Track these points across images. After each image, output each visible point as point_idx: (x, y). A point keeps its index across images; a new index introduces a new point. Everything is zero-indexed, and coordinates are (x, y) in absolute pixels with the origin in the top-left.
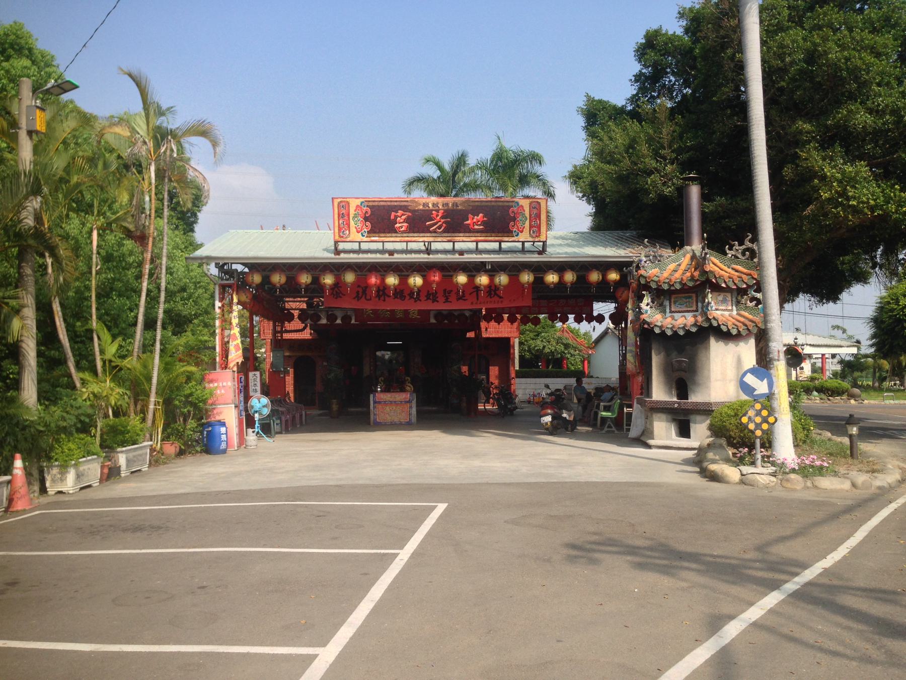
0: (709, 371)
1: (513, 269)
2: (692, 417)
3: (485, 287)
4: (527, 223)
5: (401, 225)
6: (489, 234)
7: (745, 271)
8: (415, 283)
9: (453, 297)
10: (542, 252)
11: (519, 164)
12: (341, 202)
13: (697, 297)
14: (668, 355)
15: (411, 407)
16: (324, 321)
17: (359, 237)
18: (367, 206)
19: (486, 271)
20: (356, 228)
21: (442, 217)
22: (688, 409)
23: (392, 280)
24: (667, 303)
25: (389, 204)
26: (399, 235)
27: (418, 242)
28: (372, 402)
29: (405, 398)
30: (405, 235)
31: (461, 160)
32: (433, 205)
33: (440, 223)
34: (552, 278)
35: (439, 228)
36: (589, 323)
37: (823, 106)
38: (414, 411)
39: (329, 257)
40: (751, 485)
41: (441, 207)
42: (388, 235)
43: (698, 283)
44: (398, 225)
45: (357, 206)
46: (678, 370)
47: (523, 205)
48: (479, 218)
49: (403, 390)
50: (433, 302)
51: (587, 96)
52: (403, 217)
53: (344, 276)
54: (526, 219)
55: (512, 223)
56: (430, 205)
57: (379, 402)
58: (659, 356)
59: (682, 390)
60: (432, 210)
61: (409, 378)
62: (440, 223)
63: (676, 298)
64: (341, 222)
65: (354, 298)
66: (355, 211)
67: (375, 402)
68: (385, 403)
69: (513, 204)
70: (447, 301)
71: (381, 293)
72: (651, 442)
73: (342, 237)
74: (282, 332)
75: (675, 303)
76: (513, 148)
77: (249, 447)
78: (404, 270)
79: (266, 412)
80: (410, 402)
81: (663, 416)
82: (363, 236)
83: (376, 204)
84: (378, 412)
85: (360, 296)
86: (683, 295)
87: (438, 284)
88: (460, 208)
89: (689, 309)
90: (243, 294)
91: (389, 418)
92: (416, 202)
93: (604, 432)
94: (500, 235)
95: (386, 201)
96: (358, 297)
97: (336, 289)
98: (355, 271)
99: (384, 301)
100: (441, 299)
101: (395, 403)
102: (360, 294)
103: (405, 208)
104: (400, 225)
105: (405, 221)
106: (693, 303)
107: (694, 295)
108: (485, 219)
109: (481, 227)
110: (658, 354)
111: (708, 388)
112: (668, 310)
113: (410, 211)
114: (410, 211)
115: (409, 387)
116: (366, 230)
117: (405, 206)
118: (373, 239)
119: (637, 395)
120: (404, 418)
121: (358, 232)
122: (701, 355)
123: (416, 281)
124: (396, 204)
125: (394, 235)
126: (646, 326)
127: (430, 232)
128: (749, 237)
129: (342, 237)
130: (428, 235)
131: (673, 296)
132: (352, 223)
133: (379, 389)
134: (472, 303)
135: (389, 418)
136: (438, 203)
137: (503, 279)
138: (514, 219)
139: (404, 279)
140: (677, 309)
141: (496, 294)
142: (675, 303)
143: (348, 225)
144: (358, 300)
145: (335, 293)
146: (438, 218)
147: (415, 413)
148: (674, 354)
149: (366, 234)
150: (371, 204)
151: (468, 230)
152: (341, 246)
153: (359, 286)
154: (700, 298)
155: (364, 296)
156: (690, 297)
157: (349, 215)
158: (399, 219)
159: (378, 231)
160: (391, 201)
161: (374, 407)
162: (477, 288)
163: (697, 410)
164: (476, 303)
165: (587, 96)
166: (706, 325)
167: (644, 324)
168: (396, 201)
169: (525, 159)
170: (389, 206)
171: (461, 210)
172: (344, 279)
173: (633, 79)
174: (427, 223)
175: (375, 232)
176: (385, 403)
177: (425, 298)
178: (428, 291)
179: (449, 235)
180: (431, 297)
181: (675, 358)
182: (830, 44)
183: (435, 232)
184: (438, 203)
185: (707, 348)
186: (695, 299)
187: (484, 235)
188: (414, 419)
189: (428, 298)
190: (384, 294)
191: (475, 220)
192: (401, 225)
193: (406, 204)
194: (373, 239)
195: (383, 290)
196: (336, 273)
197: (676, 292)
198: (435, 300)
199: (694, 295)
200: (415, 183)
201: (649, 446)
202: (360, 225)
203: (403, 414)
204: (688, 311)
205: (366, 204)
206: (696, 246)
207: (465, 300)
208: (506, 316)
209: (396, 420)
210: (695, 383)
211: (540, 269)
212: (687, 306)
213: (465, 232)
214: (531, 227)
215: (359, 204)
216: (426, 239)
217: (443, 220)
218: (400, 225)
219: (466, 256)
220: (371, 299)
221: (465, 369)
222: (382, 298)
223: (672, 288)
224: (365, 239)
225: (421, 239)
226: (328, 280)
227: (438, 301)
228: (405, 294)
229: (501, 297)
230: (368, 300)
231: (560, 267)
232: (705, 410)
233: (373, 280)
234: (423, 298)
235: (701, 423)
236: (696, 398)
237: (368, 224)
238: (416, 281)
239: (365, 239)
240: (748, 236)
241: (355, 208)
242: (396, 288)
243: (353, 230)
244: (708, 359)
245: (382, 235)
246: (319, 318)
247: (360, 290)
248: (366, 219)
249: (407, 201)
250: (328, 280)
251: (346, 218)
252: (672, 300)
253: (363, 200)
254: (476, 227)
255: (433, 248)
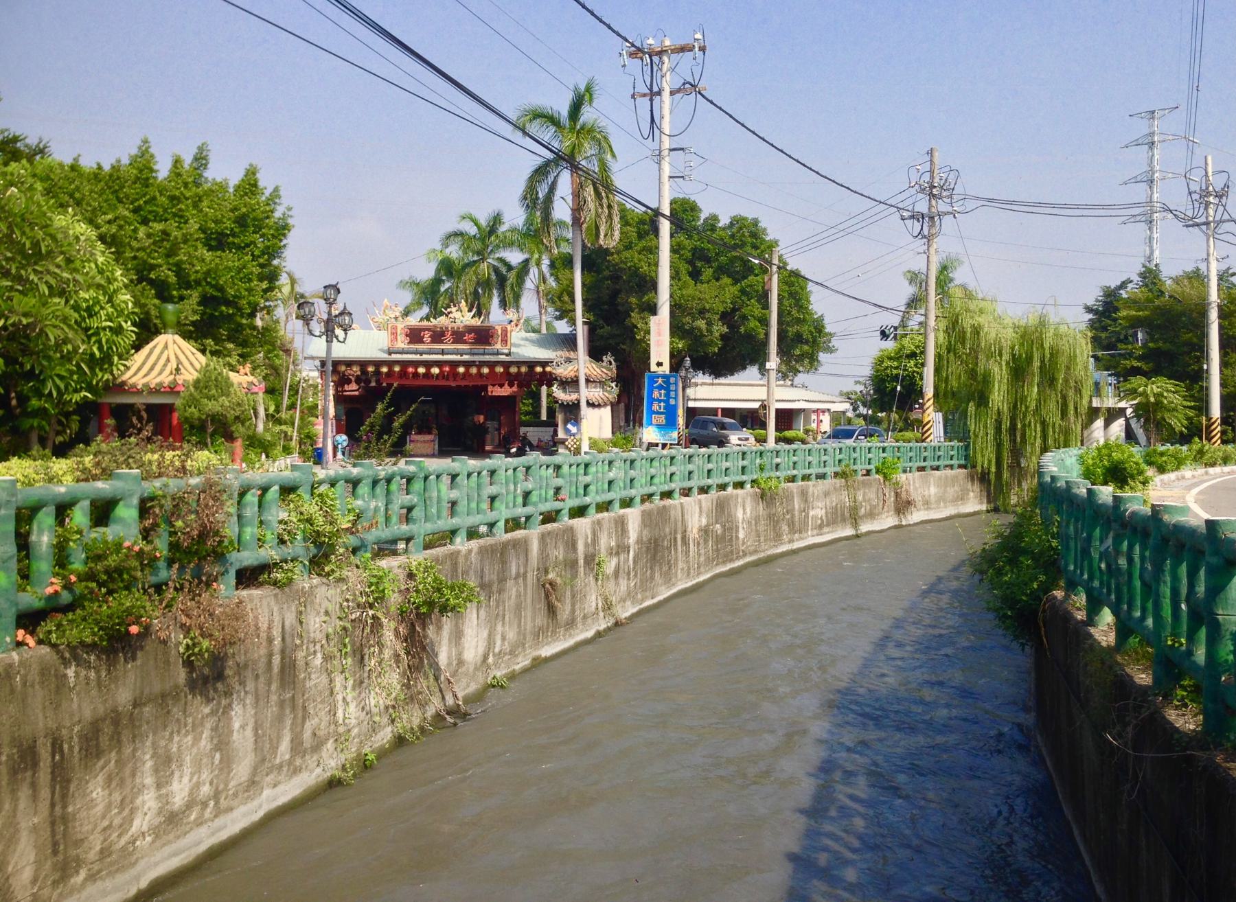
5: (427, 338)
10: (508, 355)
16: (373, 384)
19: (476, 366)
31: (497, 220)
37: (189, 563)
38: (437, 446)
39: (385, 356)
49: (430, 433)
74: (343, 391)
79: (345, 444)
100: (451, 379)
101: (424, 442)
115: (435, 431)
120: (430, 451)
123: (435, 370)
132: (399, 338)
137: (486, 370)
162: (471, 375)
182: (643, 263)
188: (436, 452)
192: (427, 338)
195: (416, 374)
200: (452, 238)
211: (507, 365)
221: (482, 418)
226: (385, 370)
231: (518, 364)
233: (411, 370)
238: (435, 370)
242: (424, 374)
246: (370, 382)
248: (407, 336)
250: (385, 370)
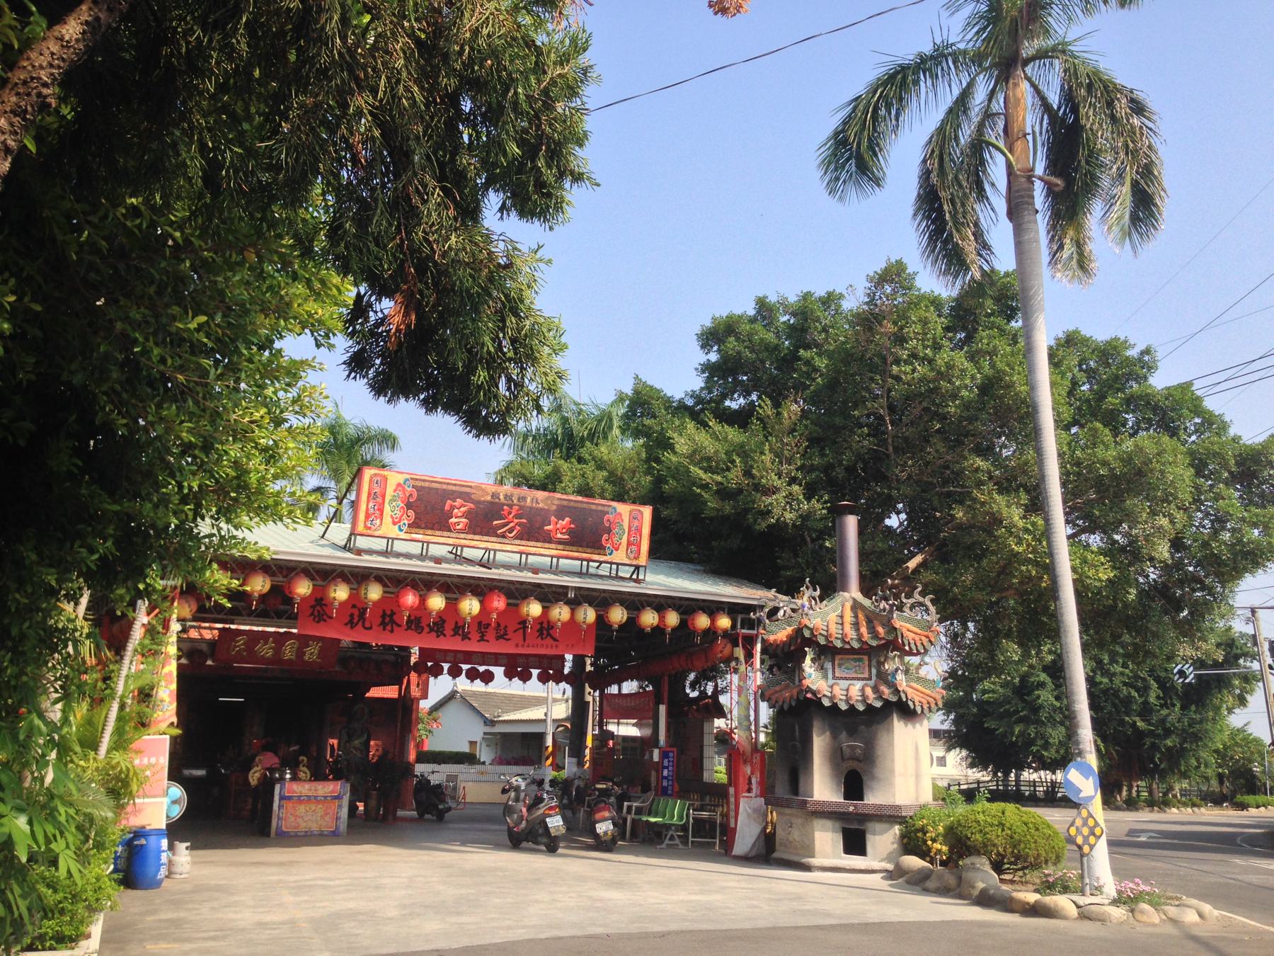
0: (893, 761)
1: (602, 601)
2: (871, 826)
3: (535, 619)
4: (625, 537)
5: (458, 520)
6: (574, 548)
7: (919, 631)
8: (471, 609)
9: (491, 634)
11: (363, 444)
12: (376, 475)
13: (870, 661)
14: (835, 736)
15: (340, 806)
17: (394, 531)
18: (413, 487)
20: (392, 517)
21: (516, 516)
22: (867, 815)
23: (437, 602)
24: (828, 665)
25: (445, 487)
26: (454, 535)
27: (476, 548)
28: (276, 798)
29: (333, 791)
30: (462, 536)
32: (506, 496)
33: (512, 525)
34: (649, 618)
35: (511, 531)
36: (557, 683)
40: (1099, 920)
41: (515, 501)
42: (438, 533)
43: (883, 642)
44: (453, 520)
45: (399, 485)
46: (848, 759)
47: (622, 512)
48: (564, 523)
50: (438, 636)
51: (637, 377)
52: (462, 509)
53: (366, 589)
54: (624, 533)
55: (605, 536)
56: (502, 497)
57: (289, 798)
58: (822, 737)
59: (854, 785)
60: (504, 504)
61: (305, 759)
62: (512, 525)
63: (842, 659)
64: (371, 505)
65: (346, 624)
66: (395, 491)
67: (282, 798)
68: (300, 800)
69: (610, 510)
70: (482, 639)
71: (387, 619)
72: (815, 861)
73: (370, 528)
75: (840, 666)
76: (355, 421)
77: (178, 876)
78: (454, 588)
80: (339, 797)
81: (829, 823)
82: (401, 530)
83: (426, 484)
84: (284, 815)
85: (355, 621)
86: (852, 657)
87: (500, 614)
88: (541, 505)
89: (859, 676)
90: (187, 605)
91: (303, 825)
92: (483, 490)
93: (664, 846)
94: (589, 550)
95: (440, 483)
96: (351, 623)
97: (318, 608)
98: (312, 579)
99: (392, 631)
100: (475, 636)
102: (356, 619)
103: (466, 497)
104: (456, 520)
105: (465, 515)
106: (864, 668)
107: (866, 658)
108: (572, 526)
109: (566, 537)
110: (819, 736)
111: (892, 784)
112: (830, 675)
113: (473, 502)
114: (473, 502)
116: (406, 522)
117: (468, 494)
118: (414, 536)
119: (743, 792)
120: (327, 824)
121: (395, 523)
122: (882, 739)
124: (454, 488)
125: (446, 534)
126: (809, 695)
127: (498, 536)
128: (919, 589)
129: (370, 528)
130: (494, 539)
131: (838, 657)
132: (387, 508)
133: (288, 776)
134: (517, 645)
135: (303, 825)
136: (512, 495)
138: (609, 531)
139: (513, 607)
140: (844, 675)
141: (549, 634)
142: (840, 666)
143: (381, 511)
144: (352, 628)
145: (316, 613)
146: (511, 516)
147: (346, 816)
148: (844, 735)
149: (405, 528)
150: (419, 484)
151: (547, 539)
152: (361, 542)
153: (354, 606)
154: (874, 662)
155: (360, 623)
156: (860, 660)
157: (384, 496)
158: (456, 511)
159: (423, 525)
160: (448, 484)
161: (280, 807)
163: (877, 815)
164: (523, 646)
165: (637, 377)
166: (894, 699)
167: (807, 692)
168: (455, 485)
169: (370, 440)
170: (444, 490)
171: (542, 509)
172: (366, 594)
173: (700, 367)
174: (495, 522)
175: (419, 527)
176: (300, 800)
177: (452, 633)
178: (457, 623)
179: (523, 542)
180: (460, 632)
181: (847, 743)
183: (504, 536)
184: (512, 495)
185: (890, 730)
186: (867, 663)
187: (567, 548)
188: (343, 826)
189: (456, 634)
190: (393, 622)
191: (558, 526)
192: (458, 520)
193: (468, 490)
194: (414, 536)
196: (355, 586)
197: (852, 651)
198: (465, 637)
199: (866, 658)
201: (807, 868)
202: (399, 514)
203: (327, 818)
204: (858, 679)
205: (412, 483)
206: (854, 591)
207: (508, 640)
208: (446, 666)
209: (315, 827)
210: (873, 778)
212: (856, 672)
213: (544, 541)
214: (629, 544)
215: (402, 482)
216: (489, 545)
217: (516, 521)
218: (456, 520)
219: (541, 575)
220: (371, 628)
222: (389, 628)
223: (847, 646)
224: (403, 535)
225: (483, 545)
226: (341, 593)
227: (470, 639)
228: (424, 624)
229: (555, 640)
230: (366, 628)
232: (890, 816)
233: (410, 599)
234: (449, 632)
235: (881, 833)
236: (874, 798)
237: (411, 513)
238: (470, 606)
239: (403, 535)
240: (917, 588)
241: (394, 487)
243: (387, 519)
244: (892, 745)
245: (429, 532)
247: (356, 613)
248: (409, 506)
249: (471, 487)
251: (379, 500)
252: (836, 663)
253: (408, 476)
254: (559, 536)
255: (464, 555)
